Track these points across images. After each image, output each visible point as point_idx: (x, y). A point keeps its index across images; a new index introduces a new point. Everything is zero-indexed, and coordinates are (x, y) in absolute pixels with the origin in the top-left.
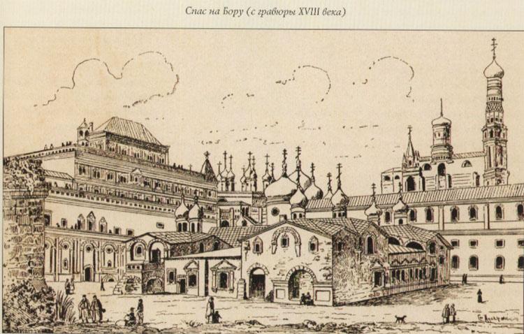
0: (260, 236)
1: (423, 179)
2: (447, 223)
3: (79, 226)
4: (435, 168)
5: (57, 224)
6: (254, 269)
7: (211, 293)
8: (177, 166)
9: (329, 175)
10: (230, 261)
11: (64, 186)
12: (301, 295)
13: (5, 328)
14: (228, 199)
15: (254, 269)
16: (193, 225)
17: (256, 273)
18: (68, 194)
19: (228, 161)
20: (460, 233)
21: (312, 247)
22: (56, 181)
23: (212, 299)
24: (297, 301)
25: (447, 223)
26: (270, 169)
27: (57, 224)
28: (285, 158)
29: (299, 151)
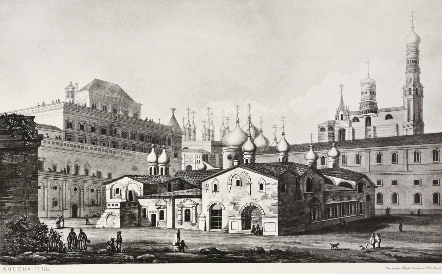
0: (217, 177)
1: (353, 129)
2: (410, 165)
3: (66, 171)
4: (363, 121)
5: (49, 168)
6: (213, 205)
7: (177, 226)
8: (148, 120)
9: (204, 122)
10: (193, 199)
11: (54, 137)
12: (252, 227)
13: (391, 212)
14: (190, 148)
15: (213, 205)
16: (151, 168)
17: (215, 208)
18: (49, 143)
19: (191, 115)
20: (385, 173)
21: (261, 187)
22: (47, 132)
23: (179, 230)
24: (249, 231)
25: (410, 165)
26: (225, 122)
27: (49, 168)
28: (237, 115)
29: (249, 106)
